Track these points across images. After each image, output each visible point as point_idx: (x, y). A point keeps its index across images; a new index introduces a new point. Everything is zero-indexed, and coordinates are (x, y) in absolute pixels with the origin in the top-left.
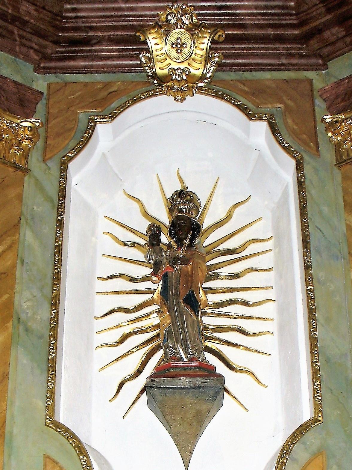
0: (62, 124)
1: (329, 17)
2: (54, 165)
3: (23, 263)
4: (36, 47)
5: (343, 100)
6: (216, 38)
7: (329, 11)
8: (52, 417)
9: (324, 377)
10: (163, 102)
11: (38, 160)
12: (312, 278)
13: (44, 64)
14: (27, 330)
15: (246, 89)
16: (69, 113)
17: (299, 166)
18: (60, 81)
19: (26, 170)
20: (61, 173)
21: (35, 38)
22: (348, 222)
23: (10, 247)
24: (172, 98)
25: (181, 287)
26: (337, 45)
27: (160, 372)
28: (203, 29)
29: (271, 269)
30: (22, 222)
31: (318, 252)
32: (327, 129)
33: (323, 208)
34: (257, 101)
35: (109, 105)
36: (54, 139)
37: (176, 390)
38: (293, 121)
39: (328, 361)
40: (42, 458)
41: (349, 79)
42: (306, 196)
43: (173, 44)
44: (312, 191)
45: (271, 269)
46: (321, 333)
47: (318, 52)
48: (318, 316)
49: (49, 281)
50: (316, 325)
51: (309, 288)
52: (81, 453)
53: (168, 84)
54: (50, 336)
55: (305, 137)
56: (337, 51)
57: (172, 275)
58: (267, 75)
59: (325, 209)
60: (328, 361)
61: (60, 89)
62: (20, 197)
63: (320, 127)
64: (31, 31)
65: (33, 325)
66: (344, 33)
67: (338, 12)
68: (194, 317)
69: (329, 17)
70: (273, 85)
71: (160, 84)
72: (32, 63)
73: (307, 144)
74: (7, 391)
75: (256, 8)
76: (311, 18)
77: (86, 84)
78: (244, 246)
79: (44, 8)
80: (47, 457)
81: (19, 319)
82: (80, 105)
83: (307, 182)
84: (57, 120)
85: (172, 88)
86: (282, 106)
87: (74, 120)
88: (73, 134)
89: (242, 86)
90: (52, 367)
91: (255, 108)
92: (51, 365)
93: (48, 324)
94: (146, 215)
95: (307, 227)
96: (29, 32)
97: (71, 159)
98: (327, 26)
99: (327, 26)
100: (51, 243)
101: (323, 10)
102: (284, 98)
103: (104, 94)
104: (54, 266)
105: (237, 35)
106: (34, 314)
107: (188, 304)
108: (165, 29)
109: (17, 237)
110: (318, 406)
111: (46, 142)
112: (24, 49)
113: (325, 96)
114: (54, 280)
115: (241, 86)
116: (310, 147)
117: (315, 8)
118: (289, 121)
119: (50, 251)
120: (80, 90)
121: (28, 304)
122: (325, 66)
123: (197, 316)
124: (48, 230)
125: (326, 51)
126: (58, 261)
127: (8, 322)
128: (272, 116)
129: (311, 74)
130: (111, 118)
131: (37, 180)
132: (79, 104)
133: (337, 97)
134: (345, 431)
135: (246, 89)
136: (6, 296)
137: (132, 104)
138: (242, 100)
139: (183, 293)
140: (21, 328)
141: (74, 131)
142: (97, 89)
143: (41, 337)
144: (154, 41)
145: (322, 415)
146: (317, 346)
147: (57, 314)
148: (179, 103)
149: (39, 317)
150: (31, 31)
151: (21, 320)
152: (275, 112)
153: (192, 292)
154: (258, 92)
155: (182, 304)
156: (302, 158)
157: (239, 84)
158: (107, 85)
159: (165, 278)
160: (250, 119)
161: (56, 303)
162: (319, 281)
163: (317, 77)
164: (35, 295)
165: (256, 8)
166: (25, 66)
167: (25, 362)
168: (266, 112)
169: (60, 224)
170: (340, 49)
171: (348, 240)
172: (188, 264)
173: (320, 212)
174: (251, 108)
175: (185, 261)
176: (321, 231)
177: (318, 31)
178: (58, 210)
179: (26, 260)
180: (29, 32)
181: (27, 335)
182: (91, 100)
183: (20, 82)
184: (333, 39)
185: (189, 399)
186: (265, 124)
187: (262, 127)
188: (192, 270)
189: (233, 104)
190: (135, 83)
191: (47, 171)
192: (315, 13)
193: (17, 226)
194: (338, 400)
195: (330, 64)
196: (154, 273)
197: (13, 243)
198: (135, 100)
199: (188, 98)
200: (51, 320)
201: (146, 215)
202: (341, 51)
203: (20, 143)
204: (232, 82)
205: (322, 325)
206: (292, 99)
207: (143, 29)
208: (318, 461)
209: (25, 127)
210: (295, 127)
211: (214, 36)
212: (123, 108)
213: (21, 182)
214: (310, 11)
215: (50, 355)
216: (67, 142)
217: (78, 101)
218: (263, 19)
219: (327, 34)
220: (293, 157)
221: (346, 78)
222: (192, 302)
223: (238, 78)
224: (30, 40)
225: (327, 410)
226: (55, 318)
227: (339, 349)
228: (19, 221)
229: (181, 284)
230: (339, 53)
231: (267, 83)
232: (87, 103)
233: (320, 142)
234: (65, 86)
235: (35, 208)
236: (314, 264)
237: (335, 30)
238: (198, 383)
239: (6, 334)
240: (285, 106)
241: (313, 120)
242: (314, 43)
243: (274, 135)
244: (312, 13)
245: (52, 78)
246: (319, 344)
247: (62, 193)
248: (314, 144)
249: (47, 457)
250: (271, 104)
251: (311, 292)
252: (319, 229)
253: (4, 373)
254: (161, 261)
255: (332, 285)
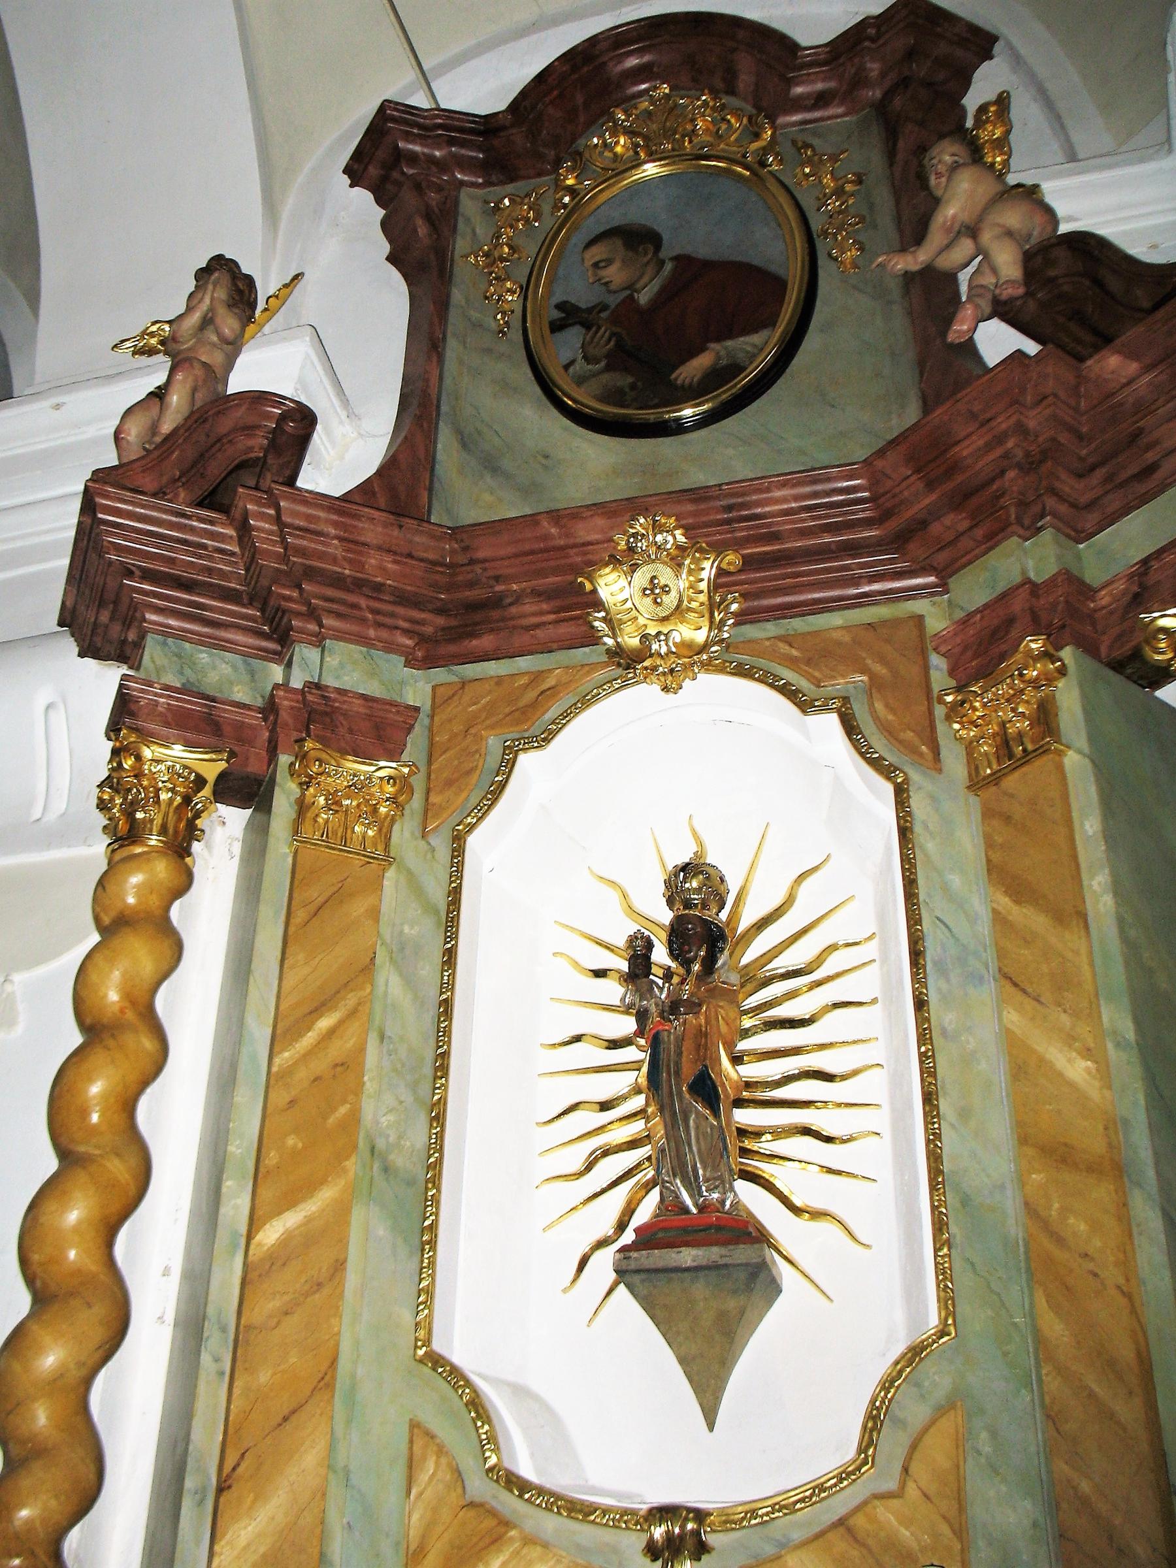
0: (456, 762)
1: (933, 497)
2: (441, 844)
3: (382, 1037)
4: (405, 625)
5: (976, 656)
6: (724, 566)
7: (930, 485)
8: (427, 1342)
9: (958, 1238)
10: (643, 696)
11: (413, 834)
12: (929, 1028)
13: (428, 654)
14: (386, 1169)
15: (795, 653)
16: (469, 739)
17: (901, 795)
18: (454, 679)
19: (388, 859)
20: (453, 857)
21: (400, 610)
22: (995, 906)
23: (353, 1013)
24: (656, 688)
25: (684, 1059)
26: (959, 545)
27: (648, 1238)
28: (697, 555)
29: (874, 1001)
30: (378, 961)
31: (943, 972)
32: (949, 718)
33: (951, 877)
34: (817, 674)
35: (533, 721)
36: (441, 792)
37: (673, 1275)
38: (887, 706)
39: (965, 1201)
40: (405, 1429)
41: (981, 612)
42: (914, 858)
43: (645, 589)
44: (927, 844)
45: (874, 1001)
46: (949, 1143)
47: (928, 561)
48: (944, 1105)
49: (428, 1071)
50: (939, 1129)
51: (923, 1049)
52: (479, 1416)
53: (647, 663)
54: (427, 1181)
55: (909, 735)
56: (962, 556)
57: (669, 1037)
58: (836, 619)
59: (955, 880)
60: (965, 1201)
61: (453, 695)
62: (375, 914)
63: (940, 711)
64: (392, 599)
65: (398, 1160)
66: (966, 524)
67: (950, 485)
68: (711, 1119)
69: (933, 497)
70: (847, 638)
71: (629, 663)
72: (401, 654)
73: (913, 750)
74: (341, 1295)
75: (796, 498)
76: (902, 502)
77: (499, 680)
78: (818, 961)
79: (410, 556)
80: (414, 1425)
81: (373, 1149)
82: (488, 722)
83: (918, 828)
84: (448, 755)
85: (654, 668)
86: (865, 678)
87: (477, 751)
88: (474, 781)
89: (787, 647)
90: (429, 1243)
91: (812, 687)
92: (425, 1240)
93: (424, 1155)
94: (631, 911)
95: (919, 922)
96: (390, 602)
97: (472, 827)
98: (933, 514)
99: (933, 514)
100: (432, 994)
101: (920, 485)
102: (869, 661)
103: (531, 695)
104: (438, 1042)
105: (766, 553)
106: (400, 1137)
107: (699, 1095)
108: (628, 561)
109: (368, 990)
110: (947, 1299)
111: (427, 800)
112: (384, 634)
113: (943, 649)
114: (436, 1069)
115: (784, 648)
116: (921, 755)
117: (904, 484)
118: (879, 706)
119: (431, 1012)
120: (490, 692)
121: (391, 1117)
122: (943, 587)
123: (716, 1113)
124: (429, 970)
125: (941, 558)
126: (444, 1032)
127: (348, 1157)
128: (846, 700)
129: (919, 606)
130: (544, 740)
131: (409, 872)
132: (486, 718)
133: (966, 648)
134: (1005, 1354)
135: (795, 653)
136: (343, 1110)
137: (582, 710)
138: (788, 675)
139: (689, 1071)
140: (376, 1166)
141: (478, 772)
142: (518, 687)
143: (411, 1183)
144: (612, 587)
145: (954, 1321)
146: (942, 1172)
147: (440, 1136)
148: (671, 695)
149: (408, 1144)
150: (392, 599)
151: (376, 1150)
152: (852, 691)
153: (706, 1067)
154: (819, 655)
155: (687, 1096)
156: (906, 780)
157: (781, 645)
158: (537, 676)
159: (655, 1044)
160: (804, 712)
161: (438, 1114)
162: (944, 1032)
163: (933, 609)
164: (402, 1099)
165: (796, 498)
166: (388, 661)
167: (381, 1232)
168: (835, 694)
169: (450, 958)
170: (967, 553)
171: (996, 944)
172: (697, 1013)
173: (946, 888)
174: (806, 692)
175: (694, 1006)
176: (947, 927)
177: (921, 525)
178: (446, 931)
179: (388, 1033)
180: (390, 602)
181: (387, 1180)
182: (507, 710)
183: (377, 695)
184: (950, 536)
185: (700, 1289)
186: (834, 718)
187: (831, 722)
188: (707, 1022)
189: (772, 686)
190: (587, 668)
191: (429, 856)
192: (906, 493)
193: (368, 968)
194: (989, 1287)
195: (952, 582)
196: (640, 1033)
197: (359, 1004)
198: (586, 702)
199: (687, 683)
200: (429, 1149)
201: (631, 911)
202: (968, 557)
203: (375, 810)
204: (767, 643)
205: (953, 1126)
206: (882, 660)
207: (590, 567)
208: (946, 1424)
209: (381, 779)
210: (891, 717)
211: (721, 562)
212: (567, 715)
213: (376, 885)
214: (897, 490)
215: (425, 1219)
216: (464, 795)
217: (484, 715)
218: (813, 518)
219: (935, 528)
220: (889, 778)
221: (977, 611)
222: (706, 1089)
223: (782, 632)
224: (392, 615)
225: (964, 1308)
226: (437, 1145)
227: (988, 1176)
228: (373, 959)
229: (685, 1054)
230: (964, 560)
231: (835, 635)
232: (501, 716)
233: (942, 742)
234: (463, 687)
235: (406, 929)
236: (933, 998)
237: (948, 520)
238: (715, 1257)
239: (343, 1182)
240: (871, 679)
241: (925, 698)
242: (915, 548)
243: (850, 739)
244: (901, 492)
245: (440, 675)
246: (946, 1167)
247: (455, 896)
248: (928, 747)
249: (414, 1425)
250: (843, 677)
251: (928, 1058)
252: (945, 924)
253: (337, 1261)
254: (646, 1011)
255: (971, 1039)
